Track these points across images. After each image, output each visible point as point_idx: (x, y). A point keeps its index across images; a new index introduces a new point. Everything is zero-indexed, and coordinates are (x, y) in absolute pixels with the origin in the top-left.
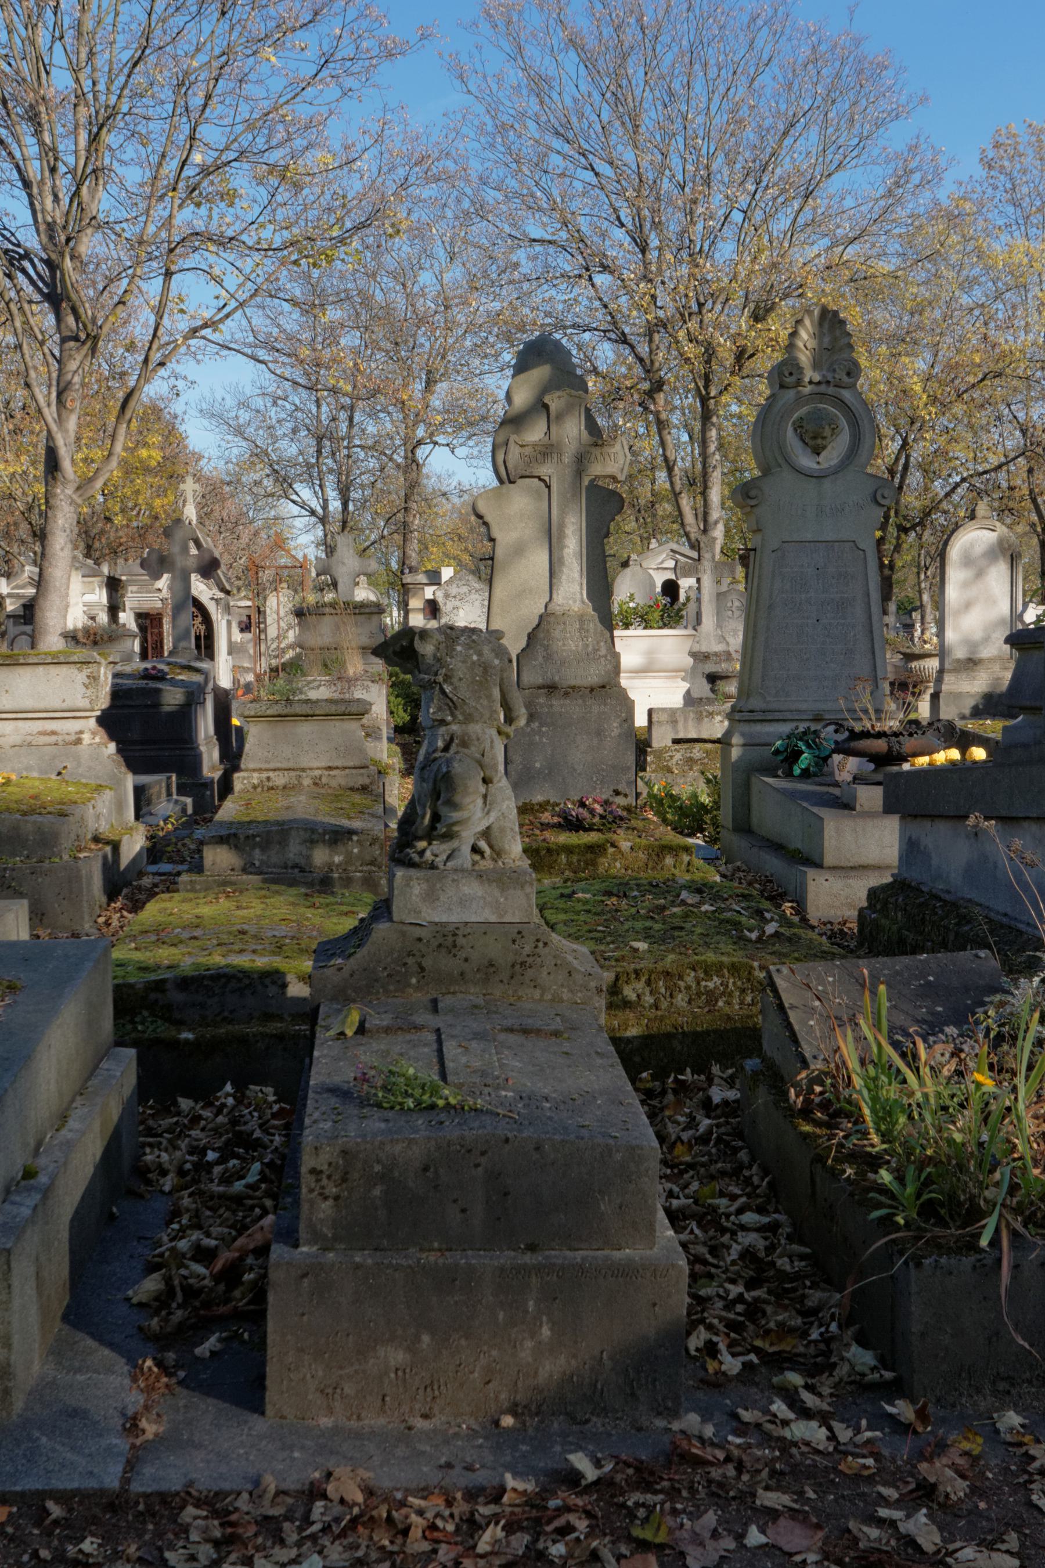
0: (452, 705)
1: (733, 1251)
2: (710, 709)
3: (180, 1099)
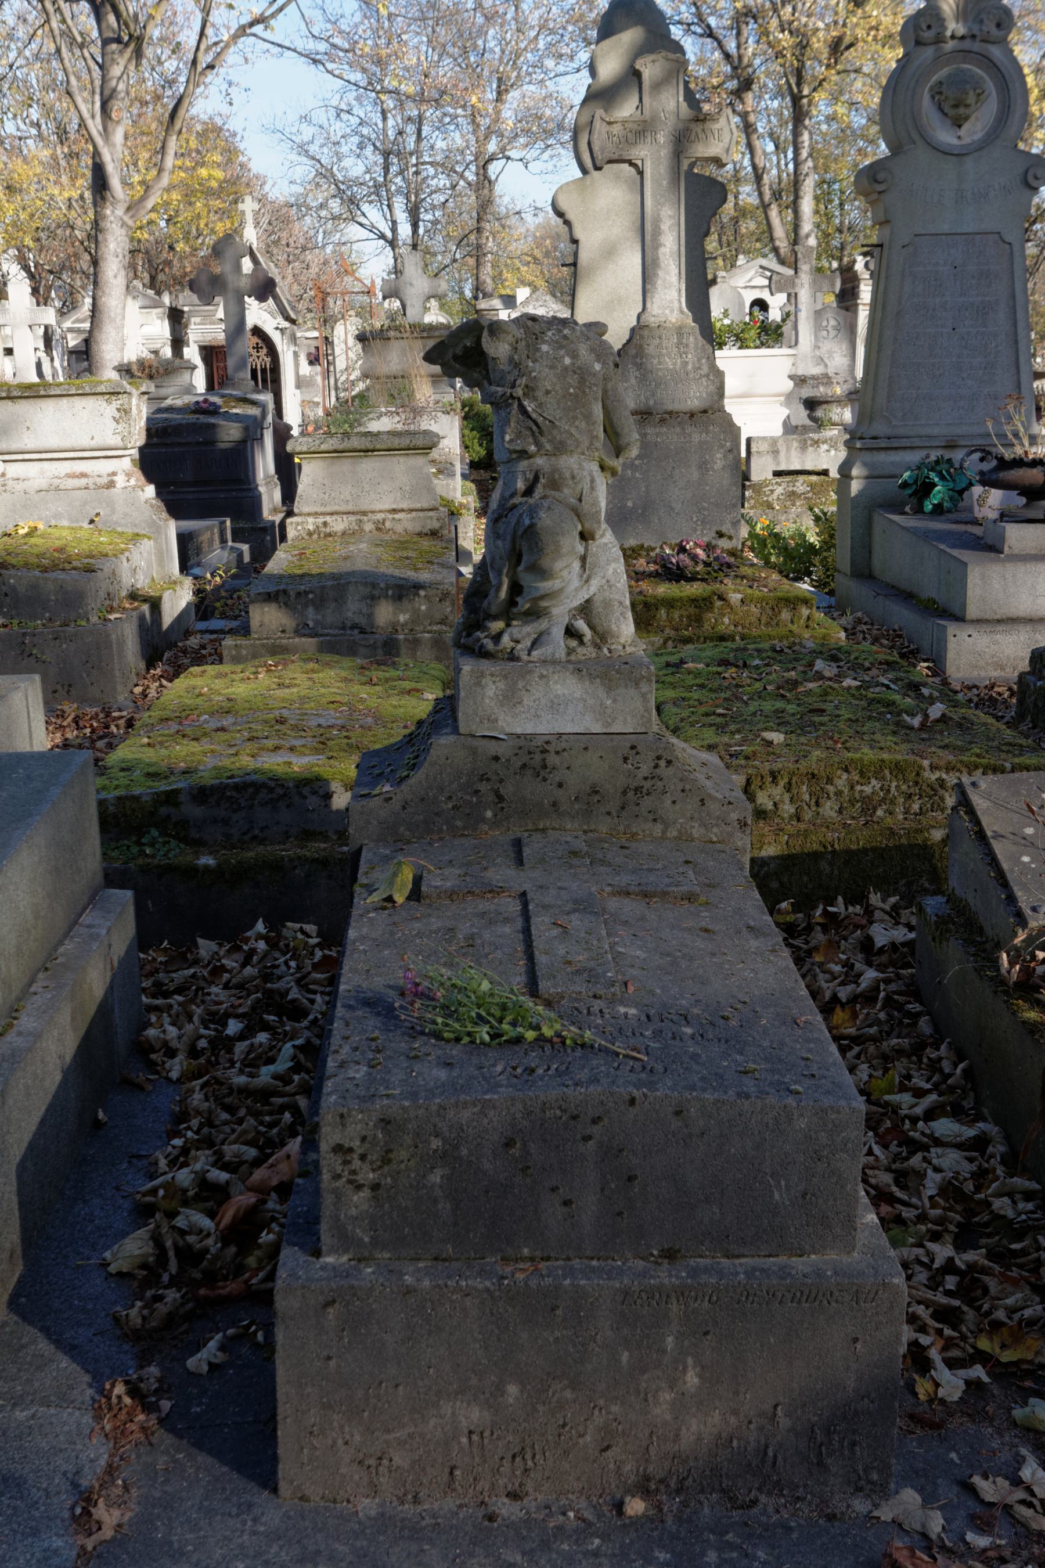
0: (536, 429)
1: (928, 1183)
2: (815, 436)
3: (200, 941)
